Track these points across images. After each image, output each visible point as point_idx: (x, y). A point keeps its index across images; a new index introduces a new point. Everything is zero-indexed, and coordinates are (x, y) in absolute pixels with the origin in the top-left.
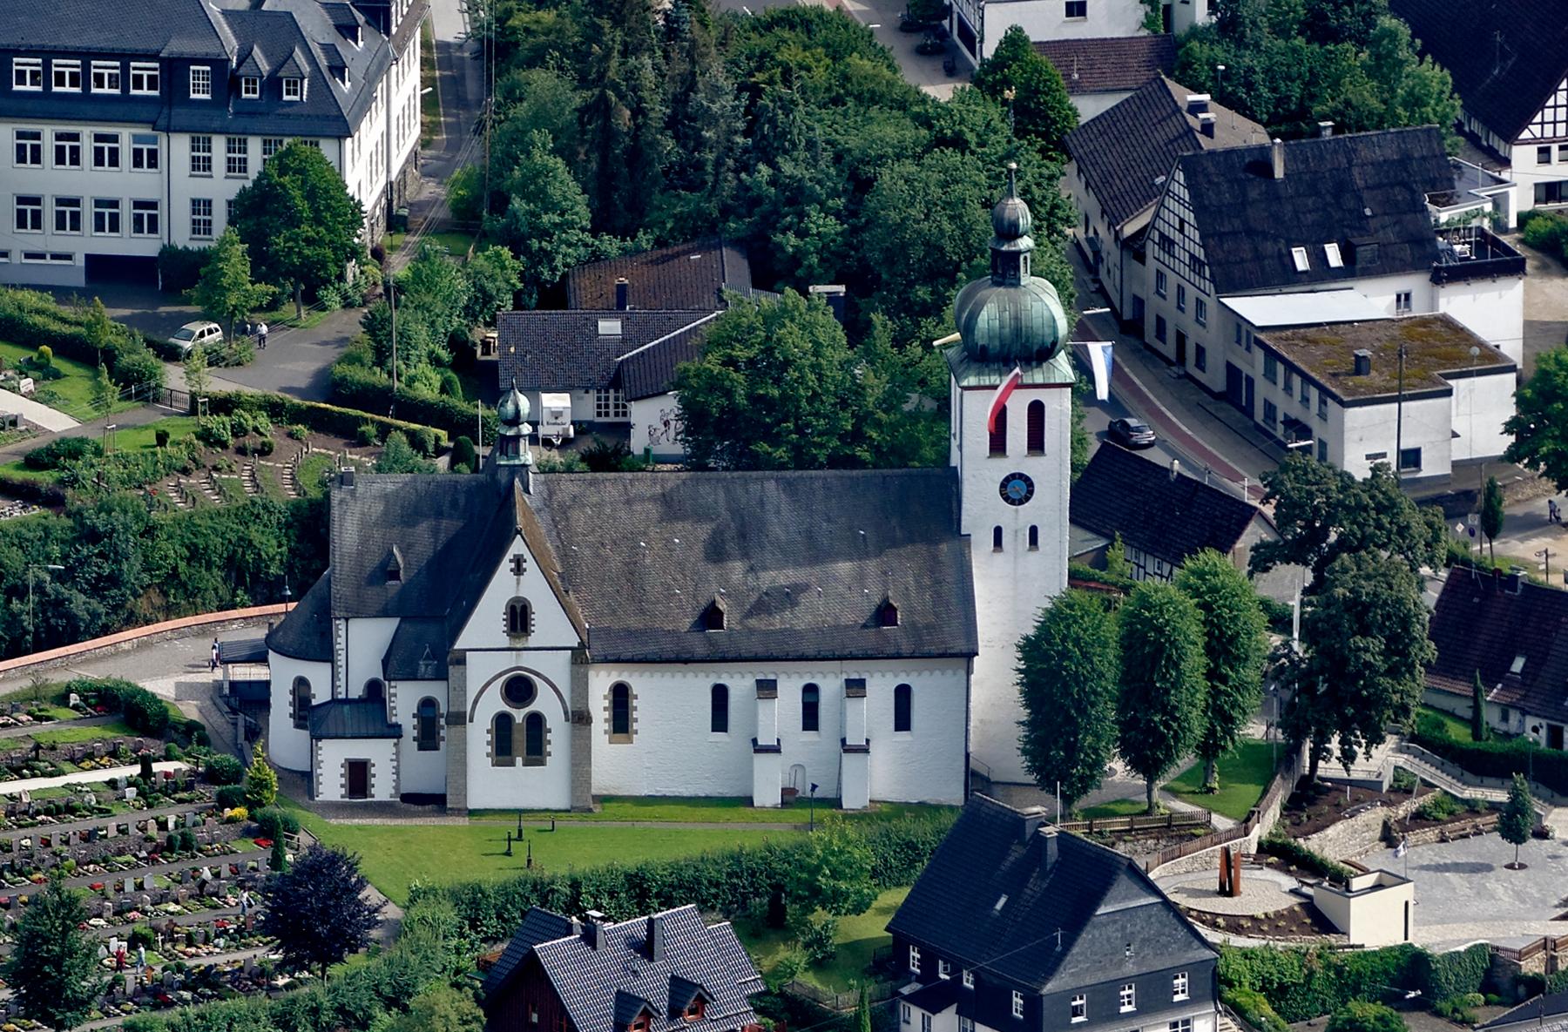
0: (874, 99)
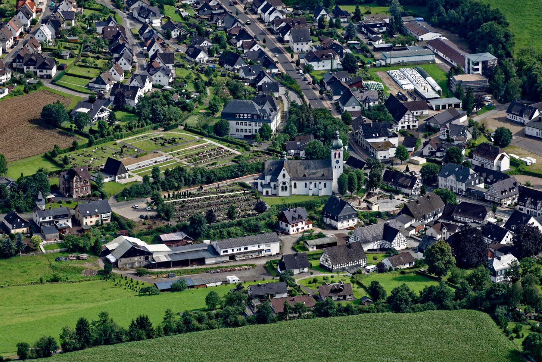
0: (328, 118)
